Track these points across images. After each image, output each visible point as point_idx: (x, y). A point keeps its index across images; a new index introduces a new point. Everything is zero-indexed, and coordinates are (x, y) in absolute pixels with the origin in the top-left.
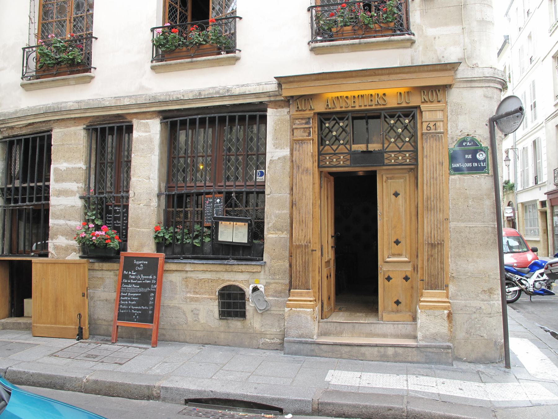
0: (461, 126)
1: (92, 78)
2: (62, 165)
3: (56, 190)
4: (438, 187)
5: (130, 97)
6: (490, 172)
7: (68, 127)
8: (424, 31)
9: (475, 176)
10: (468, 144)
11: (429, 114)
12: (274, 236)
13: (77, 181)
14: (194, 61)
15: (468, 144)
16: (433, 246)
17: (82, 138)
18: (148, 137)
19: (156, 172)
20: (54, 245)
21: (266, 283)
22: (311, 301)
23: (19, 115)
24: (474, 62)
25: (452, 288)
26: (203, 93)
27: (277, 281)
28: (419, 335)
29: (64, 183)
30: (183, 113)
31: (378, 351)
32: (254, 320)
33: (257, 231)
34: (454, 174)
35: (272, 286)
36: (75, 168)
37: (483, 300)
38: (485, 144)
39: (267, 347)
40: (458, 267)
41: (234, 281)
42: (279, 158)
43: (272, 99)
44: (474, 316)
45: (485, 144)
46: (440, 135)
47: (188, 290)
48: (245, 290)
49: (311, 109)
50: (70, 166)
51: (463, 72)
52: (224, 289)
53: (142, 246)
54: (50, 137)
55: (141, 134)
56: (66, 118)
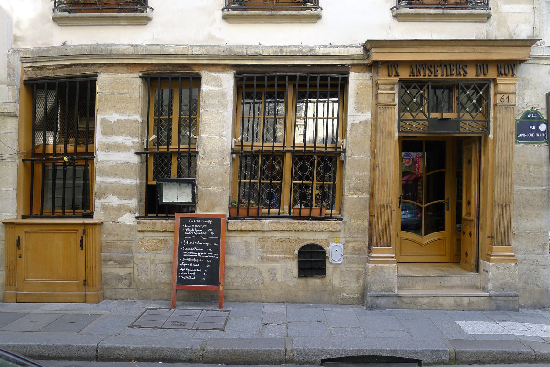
0: (527, 99)
1: (149, 19)
2: (111, 116)
3: (104, 144)
4: (508, 154)
7: (119, 73)
8: (499, 7)
9: (536, 145)
10: (532, 116)
12: (355, 196)
13: (132, 135)
14: (274, 15)
15: (532, 116)
16: (501, 206)
17: (138, 87)
18: (217, 89)
20: (102, 205)
21: (346, 241)
22: (393, 257)
23: (52, 53)
25: (514, 243)
27: (356, 239)
28: (490, 286)
29: (114, 137)
30: (259, 70)
31: (455, 301)
32: (333, 276)
34: (519, 143)
35: (351, 245)
36: (129, 121)
37: (538, 254)
39: (345, 302)
40: (519, 225)
41: (314, 240)
42: (360, 122)
43: (356, 62)
44: (532, 267)
46: (512, 107)
47: (265, 250)
48: (325, 249)
49: (397, 75)
50: (123, 118)
52: (303, 247)
53: (213, 205)
56: (118, 62)
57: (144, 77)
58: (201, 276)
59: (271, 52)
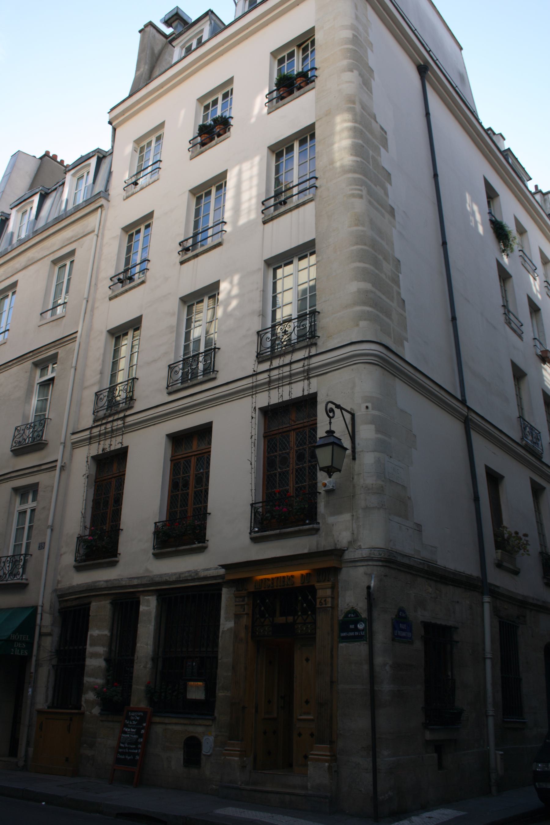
5: (138, 578)
6: (368, 640)
9: (356, 643)
10: (352, 616)
11: (323, 592)
15: (352, 616)
19: (152, 639)
24: (359, 544)
26: (182, 576)
33: (211, 690)
34: (342, 642)
38: (364, 615)
42: (228, 630)
45: (364, 615)
51: (348, 556)
54: (89, 609)
55: (146, 608)
57: (114, 604)
58: (132, 767)
59: (174, 578)
